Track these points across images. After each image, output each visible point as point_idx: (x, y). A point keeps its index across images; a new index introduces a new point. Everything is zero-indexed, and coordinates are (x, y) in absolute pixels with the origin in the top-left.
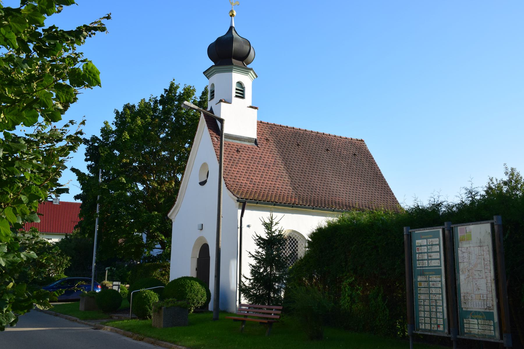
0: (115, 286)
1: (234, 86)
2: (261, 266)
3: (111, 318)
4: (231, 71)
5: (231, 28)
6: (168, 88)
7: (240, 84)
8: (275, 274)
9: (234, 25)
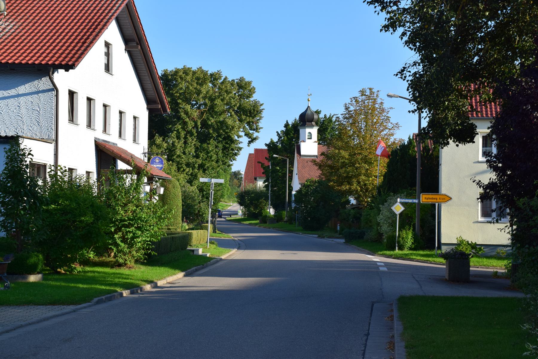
0: (44, 207)
1: (307, 134)
2: (355, 186)
3: (440, 165)
4: (305, 128)
5: (308, 107)
6: (263, 171)
7: (310, 133)
8: (439, 91)
9: (309, 105)
